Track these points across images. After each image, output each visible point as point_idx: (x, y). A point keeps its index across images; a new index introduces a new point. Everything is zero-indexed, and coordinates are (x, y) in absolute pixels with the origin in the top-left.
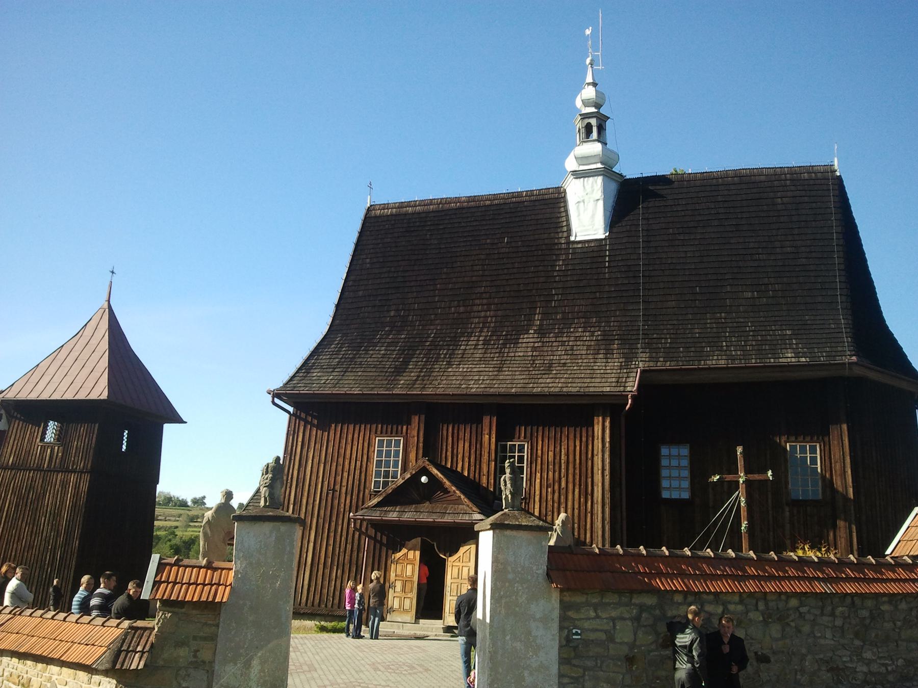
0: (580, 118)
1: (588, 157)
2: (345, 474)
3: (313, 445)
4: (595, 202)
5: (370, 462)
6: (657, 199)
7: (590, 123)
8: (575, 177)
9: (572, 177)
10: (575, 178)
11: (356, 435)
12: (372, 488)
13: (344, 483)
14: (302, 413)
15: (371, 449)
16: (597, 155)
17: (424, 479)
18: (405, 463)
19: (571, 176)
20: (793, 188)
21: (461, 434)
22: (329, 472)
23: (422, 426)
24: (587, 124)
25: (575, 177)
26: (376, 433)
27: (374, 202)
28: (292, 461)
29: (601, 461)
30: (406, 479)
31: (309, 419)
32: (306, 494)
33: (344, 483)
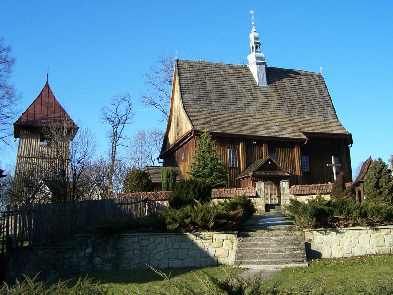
9: (256, 64)
17: (270, 163)
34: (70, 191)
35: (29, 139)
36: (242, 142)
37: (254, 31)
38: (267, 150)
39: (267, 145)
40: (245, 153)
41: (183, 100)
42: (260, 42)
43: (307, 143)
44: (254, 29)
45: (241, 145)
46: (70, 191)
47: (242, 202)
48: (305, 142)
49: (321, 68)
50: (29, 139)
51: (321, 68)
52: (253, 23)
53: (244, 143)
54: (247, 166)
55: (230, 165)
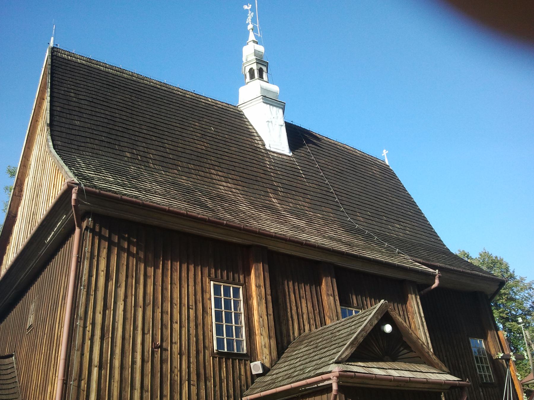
0: (255, 61)
1: (269, 91)
2: (176, 326)
3: (124, 279)
4: (280, 126)
5: (207, 313)
6: (97, 191)
7: (262, 68)
8: (264, 101)
9: (262, 100)
10: (263, 102)
11: (184, 274)
12: (215, 348)
13: (176, 338)
14: (103, 229)
15: (207, 296)
16: (276, 93)
17: (388, 328)
18: (248, 318)
19: (261, 99)
20: (269, 190)
21: (302, 292)
22: (151, 320)
23: (267, 275)
24: (250, 69)
25: (264, 101)
26: (209, 276)
27: (57, 45)
28: (92, 298)
29: (218, 360)
30: (374, 325)
31: (116, 239)
32: (118, 351)
33: (176, 338)
34: (510, 342)
35: (6, 354)
36: (257, 261)
37: (254, 41)
38: (337, 298)
39: (334, 280)
40: (269, 298)
41: (53, 129)
42: (268, 63)
43: (439, 284)
44: (252, 37)
45: (257, 277)
46: (510, 342)
47: (92, 228)
48: (434, 283)
49: (385, 152)
50: (6, 354)
51: (385, 152)
52: (250, 26)
53: (267, 267)
54: (281, 350)
55: (220, 342)
